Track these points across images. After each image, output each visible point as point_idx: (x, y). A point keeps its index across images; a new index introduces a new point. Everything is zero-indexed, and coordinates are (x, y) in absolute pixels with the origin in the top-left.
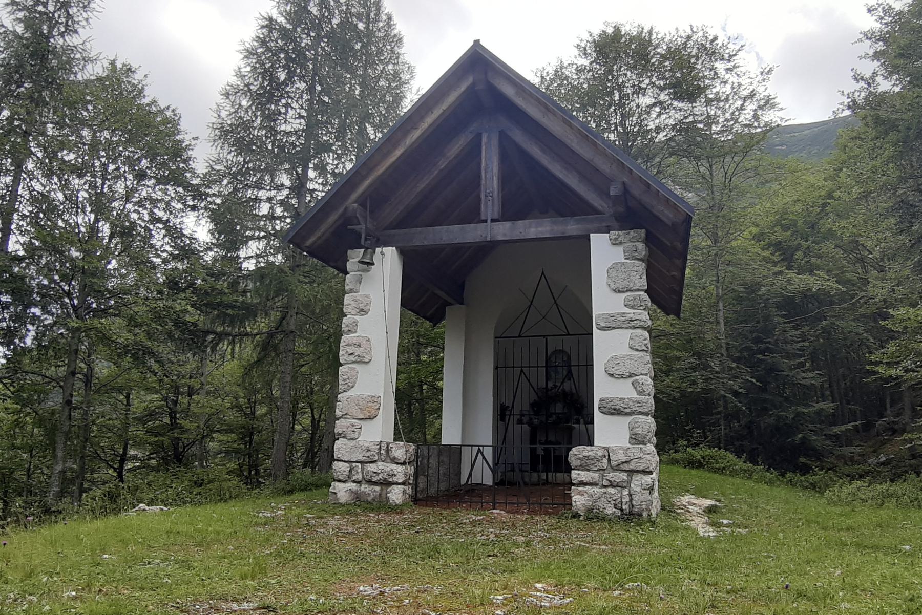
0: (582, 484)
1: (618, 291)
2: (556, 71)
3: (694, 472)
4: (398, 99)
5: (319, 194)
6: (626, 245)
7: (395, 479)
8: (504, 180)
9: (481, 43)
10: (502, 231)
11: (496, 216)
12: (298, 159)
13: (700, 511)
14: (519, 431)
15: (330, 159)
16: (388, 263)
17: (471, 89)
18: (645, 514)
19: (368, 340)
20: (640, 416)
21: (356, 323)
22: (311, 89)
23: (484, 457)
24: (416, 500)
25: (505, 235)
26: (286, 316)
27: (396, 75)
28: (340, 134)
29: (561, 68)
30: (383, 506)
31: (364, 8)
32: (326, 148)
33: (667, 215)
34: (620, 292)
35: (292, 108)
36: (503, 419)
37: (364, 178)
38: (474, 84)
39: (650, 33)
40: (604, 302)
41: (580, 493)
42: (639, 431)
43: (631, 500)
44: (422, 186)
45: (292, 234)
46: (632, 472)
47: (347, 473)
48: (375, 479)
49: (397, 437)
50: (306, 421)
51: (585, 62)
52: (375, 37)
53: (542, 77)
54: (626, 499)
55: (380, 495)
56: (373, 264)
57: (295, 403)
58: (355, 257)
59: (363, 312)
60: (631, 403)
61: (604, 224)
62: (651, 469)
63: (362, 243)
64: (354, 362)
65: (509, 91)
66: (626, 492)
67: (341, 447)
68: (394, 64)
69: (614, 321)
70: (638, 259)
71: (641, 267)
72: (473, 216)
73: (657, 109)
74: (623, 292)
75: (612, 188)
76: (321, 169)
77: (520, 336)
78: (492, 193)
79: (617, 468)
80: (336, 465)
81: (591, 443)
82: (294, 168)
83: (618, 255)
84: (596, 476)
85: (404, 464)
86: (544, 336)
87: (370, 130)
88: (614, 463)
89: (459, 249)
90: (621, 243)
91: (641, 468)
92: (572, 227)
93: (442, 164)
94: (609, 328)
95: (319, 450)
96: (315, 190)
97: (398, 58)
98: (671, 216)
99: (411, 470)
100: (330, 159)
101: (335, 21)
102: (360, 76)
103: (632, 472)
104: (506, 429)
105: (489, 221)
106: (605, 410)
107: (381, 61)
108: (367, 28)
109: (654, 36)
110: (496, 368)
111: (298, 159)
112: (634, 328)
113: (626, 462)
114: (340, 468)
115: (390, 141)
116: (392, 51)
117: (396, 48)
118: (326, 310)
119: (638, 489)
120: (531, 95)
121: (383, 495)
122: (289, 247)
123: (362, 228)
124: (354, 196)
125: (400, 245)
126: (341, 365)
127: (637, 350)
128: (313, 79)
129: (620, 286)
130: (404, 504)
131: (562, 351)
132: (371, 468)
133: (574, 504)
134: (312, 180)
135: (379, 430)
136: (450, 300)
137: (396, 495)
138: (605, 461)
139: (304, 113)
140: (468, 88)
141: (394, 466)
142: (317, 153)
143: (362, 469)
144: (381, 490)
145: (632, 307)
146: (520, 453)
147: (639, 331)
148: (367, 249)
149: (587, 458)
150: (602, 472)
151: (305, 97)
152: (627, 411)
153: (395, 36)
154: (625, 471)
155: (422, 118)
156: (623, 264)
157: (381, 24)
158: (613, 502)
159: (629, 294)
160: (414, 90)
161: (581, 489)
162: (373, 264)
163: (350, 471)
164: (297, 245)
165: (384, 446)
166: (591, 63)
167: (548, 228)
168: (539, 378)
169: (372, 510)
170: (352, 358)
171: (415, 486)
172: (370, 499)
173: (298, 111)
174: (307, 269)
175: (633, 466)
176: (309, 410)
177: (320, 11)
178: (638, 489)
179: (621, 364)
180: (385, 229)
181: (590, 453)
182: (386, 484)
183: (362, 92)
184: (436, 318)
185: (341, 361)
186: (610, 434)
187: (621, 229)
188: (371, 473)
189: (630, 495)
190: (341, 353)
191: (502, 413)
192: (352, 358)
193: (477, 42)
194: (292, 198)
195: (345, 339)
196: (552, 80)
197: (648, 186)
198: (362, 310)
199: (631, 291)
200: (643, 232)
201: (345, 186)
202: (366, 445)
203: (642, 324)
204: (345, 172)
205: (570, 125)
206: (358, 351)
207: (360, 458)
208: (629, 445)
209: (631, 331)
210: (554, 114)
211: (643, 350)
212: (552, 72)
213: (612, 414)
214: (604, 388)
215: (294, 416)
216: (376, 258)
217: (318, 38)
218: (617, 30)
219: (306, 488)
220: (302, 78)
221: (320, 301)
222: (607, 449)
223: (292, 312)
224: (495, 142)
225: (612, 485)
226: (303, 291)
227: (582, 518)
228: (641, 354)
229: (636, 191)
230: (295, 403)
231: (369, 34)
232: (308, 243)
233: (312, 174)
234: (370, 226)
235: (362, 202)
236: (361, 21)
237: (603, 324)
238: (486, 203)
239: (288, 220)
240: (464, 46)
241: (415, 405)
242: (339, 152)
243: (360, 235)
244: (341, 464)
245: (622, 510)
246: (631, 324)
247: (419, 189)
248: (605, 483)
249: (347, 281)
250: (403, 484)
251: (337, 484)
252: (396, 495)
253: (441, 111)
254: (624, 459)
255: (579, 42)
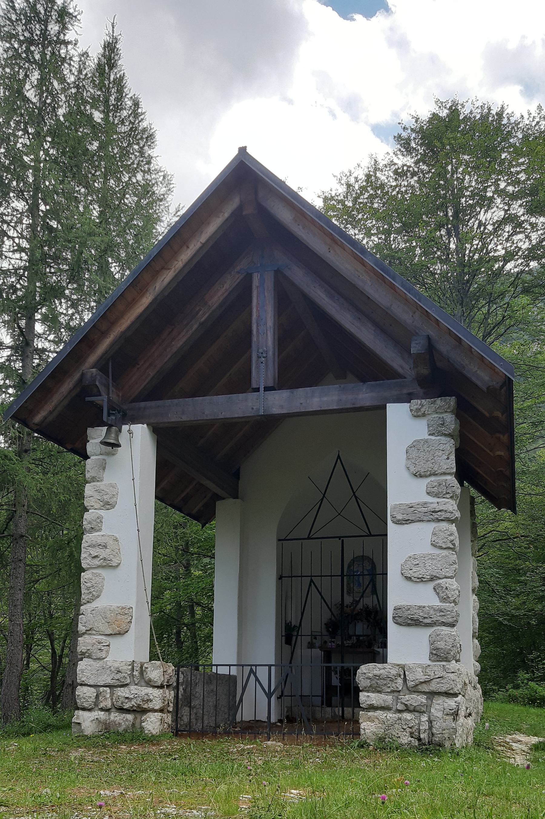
0: (372, 708)
1: (418, 475)
2: (368, 176)
3: (533, 710)
4: (151, 221)
5: (50, 354)
6: (429, 417)
7: (151, 705)
8: (283, 337)
9: (248, 151)
10: (279, 402)
11: (270, 383)
12: (20, 307)
13: (525, 749)
14: (309, 657)
15: (62, 307)
16: (138, 444)
17: (237, 214)
18: (447, 744)
19: (116, 540)
20: (444, 628)
21: (100, 520)
22: (33, 210)
23: (257, 679)
24: (177, 731)
25: (282, 407)
26: (13, 516)
27: (146, 190)
28: (75, 275)
29: (376, 170)
30: (136, 736)
31: (100, 89)
32: (54, 292)
33: (482, 378)
34: (421, 476)
35: (9, 237)
36: (288, 641)
37: (104, 334)
38: (240, 208)
39: (500, 115)
40: (403, 488)
41: (370, 719)
42: (441, 645)
43: (431, 728)
44: (178, 344)
45: (16, 408)
46: (432, 694)
47: (93, 699)
48: (126, 706)
49: (153, 657)
50: (46, 659)
51: (409, 161)
52: (116, 133)
53: (349, 185)
54: (425, 726)
55: (133, 724)
56: (119, 446)
57: (29, 632)
58: (96, 436)
59: (108, 505)
60: (432, 612)
61: (405, 391)
62: (456, 690)
63: (105, 418)
64: (99, 567)
65: (285, 216)
66: (424, 718)
67: (85, 669)
68: (144, 172)
69: (413, 512)
70: (445, 435)
71: (448, 446)
72: (243, 384)
73: (508, 228)
74: (426, 476)
75: (413, 345)
76: (52, 320)
77: (309, 538)
78: (266, 352)
79: (414, 690)
80: (81, 691)
81: (384, 660)
82: (15, 320)
83: (420, 430)
84: (389, 699)
85: (161, 687)
86: (340, 538)
87: (114, 268)
88: (410, 684)
89: (230, 426)
90: (424, 415)
91: (444, 689)
92: (365, 395)
93: (203, 315)
94: (407, 522)
95: (60, 691)
96: (44, 350)
97: (149, 163)
98: (487, 378)
99: (170, 694)
100: (62, 307)
101: (61, 112)
102: (98, 190)
103: (432, 694)
104: (292, 654)
105: (262, 389)
106: (400, 620)
107: (127, 168)
108: (106, 119)
109: (505, 121)
110: (280, 578)
111: (20, 307)
112: (438, 520)
113: (425, 682)
114: (84, 694)
115: (136, 286)
116: (141, 152)
117: (146, 148)
118: (64, 506)
119: (440, 714)
120: (313, 222)
121: (137, 725)
122: (13, 427)
123: (103, 400)
124: (93, 358)
125: (152, 421)
126: (84, 570)
127: (441, 548)
128: (35, 197)
129: (422, 467)
130: (162, 734)
131: (363, 558)
132: (122, 692)
133: (362, 732)
134: (39, 336)
135: (131, 648)
136: (219, 491)
137: (153, 724)
138: (400, 681)
139: (25, 244)
140: (233, 214)
141: (150, 690)
142: (45, 300)
143: (112, 694)
144: (135, 718)
145: (437, 495)
146: (310, 682)
147: (444, 525)
148: (110, 426)
149: (378, 677)
150: (396, 694)
151: (26, 221)
152: (426, 621)
153: (144, 130)
154: (424, 693)
155: (175, 254)
156: (426, 441)
157: (125, 113)
158: (408, 730)
159: (433, 478)
160: (172, 210)
161: (370, 714)
162: (119, 446)
163: (97, 697)
164: (24, 423)
165: (137, 667)
166: (416, 163)
167: (335, 398)
168: (332, 590)
169: (124, 742)
170: (96, 562)
171: (176, 713)
172: (121, 729)
173: (17, 240)
174: (39, 455)
175: (434, 687)
176: (47, 643)
177: (41, 95)
178: (440, 714)
179: (421, 565)
180: (133, 401)
181: (382, 671)
182: (140, 711)
183: (101, 213)
184: (205, 516)
185: (84, 566)
186: (405, 648)
187: (426, 396)
188: (122, 699)
189: (430, 722)
190: (83, 556)
191: (288, 634)
192: (96, 562)
193: (243, 151)
194: (15, 361)
195: (88, 538)
196: (363, 189)
197: (459, 340)
198: (107, 503)
199: (435, 474)
200: (452, 401)
201: (83, 342)
202: (116, 665)
203: (448, 515)
204: (82, 324)
205: (363, 263)
206: (103, 553)
207: (109, 681)
208: (429, 663)
209: (433, 525)
210: (343, 247)
211: (449, 548)
212: (362, 177)
213: (409, 625)
214: (399, 594)
215: (29, 649)
216: (123, 439)
217: (39, 137)
218: (454, 111)
219: (47, 728)
220: (20, 195)
221: (56, 495)
222: (403, 667)
223: (20, 511)
224: (269, 283)
225: (408, 709)
226: (31, 480)
227: (371, 748)
228: (445, 553)
229: (444, 347)
230: (29, 632)
231: (109, 127)
232: (38, 419)
233: (39, 328)
234: (114, 397)
235: (102, 366)
236: (97, 109)
237: (399, 517)
238: (258, 367)
239: (11, 391)
240: (231, 154)
241: (179, 628)
242: (74, 297)
243: (101, 409)
244: (85, 689)
245: (419, 740)
246: (435, 516)
247: (174, 349)
248: (400, 707)
249: (88, 467)
250: (161, 711)
251: (81, 712)
252: (153, 724)
253: (198, 245)
254: (423, 678)
255: (401, 131)
